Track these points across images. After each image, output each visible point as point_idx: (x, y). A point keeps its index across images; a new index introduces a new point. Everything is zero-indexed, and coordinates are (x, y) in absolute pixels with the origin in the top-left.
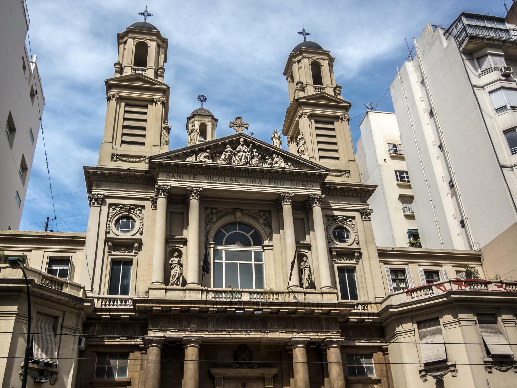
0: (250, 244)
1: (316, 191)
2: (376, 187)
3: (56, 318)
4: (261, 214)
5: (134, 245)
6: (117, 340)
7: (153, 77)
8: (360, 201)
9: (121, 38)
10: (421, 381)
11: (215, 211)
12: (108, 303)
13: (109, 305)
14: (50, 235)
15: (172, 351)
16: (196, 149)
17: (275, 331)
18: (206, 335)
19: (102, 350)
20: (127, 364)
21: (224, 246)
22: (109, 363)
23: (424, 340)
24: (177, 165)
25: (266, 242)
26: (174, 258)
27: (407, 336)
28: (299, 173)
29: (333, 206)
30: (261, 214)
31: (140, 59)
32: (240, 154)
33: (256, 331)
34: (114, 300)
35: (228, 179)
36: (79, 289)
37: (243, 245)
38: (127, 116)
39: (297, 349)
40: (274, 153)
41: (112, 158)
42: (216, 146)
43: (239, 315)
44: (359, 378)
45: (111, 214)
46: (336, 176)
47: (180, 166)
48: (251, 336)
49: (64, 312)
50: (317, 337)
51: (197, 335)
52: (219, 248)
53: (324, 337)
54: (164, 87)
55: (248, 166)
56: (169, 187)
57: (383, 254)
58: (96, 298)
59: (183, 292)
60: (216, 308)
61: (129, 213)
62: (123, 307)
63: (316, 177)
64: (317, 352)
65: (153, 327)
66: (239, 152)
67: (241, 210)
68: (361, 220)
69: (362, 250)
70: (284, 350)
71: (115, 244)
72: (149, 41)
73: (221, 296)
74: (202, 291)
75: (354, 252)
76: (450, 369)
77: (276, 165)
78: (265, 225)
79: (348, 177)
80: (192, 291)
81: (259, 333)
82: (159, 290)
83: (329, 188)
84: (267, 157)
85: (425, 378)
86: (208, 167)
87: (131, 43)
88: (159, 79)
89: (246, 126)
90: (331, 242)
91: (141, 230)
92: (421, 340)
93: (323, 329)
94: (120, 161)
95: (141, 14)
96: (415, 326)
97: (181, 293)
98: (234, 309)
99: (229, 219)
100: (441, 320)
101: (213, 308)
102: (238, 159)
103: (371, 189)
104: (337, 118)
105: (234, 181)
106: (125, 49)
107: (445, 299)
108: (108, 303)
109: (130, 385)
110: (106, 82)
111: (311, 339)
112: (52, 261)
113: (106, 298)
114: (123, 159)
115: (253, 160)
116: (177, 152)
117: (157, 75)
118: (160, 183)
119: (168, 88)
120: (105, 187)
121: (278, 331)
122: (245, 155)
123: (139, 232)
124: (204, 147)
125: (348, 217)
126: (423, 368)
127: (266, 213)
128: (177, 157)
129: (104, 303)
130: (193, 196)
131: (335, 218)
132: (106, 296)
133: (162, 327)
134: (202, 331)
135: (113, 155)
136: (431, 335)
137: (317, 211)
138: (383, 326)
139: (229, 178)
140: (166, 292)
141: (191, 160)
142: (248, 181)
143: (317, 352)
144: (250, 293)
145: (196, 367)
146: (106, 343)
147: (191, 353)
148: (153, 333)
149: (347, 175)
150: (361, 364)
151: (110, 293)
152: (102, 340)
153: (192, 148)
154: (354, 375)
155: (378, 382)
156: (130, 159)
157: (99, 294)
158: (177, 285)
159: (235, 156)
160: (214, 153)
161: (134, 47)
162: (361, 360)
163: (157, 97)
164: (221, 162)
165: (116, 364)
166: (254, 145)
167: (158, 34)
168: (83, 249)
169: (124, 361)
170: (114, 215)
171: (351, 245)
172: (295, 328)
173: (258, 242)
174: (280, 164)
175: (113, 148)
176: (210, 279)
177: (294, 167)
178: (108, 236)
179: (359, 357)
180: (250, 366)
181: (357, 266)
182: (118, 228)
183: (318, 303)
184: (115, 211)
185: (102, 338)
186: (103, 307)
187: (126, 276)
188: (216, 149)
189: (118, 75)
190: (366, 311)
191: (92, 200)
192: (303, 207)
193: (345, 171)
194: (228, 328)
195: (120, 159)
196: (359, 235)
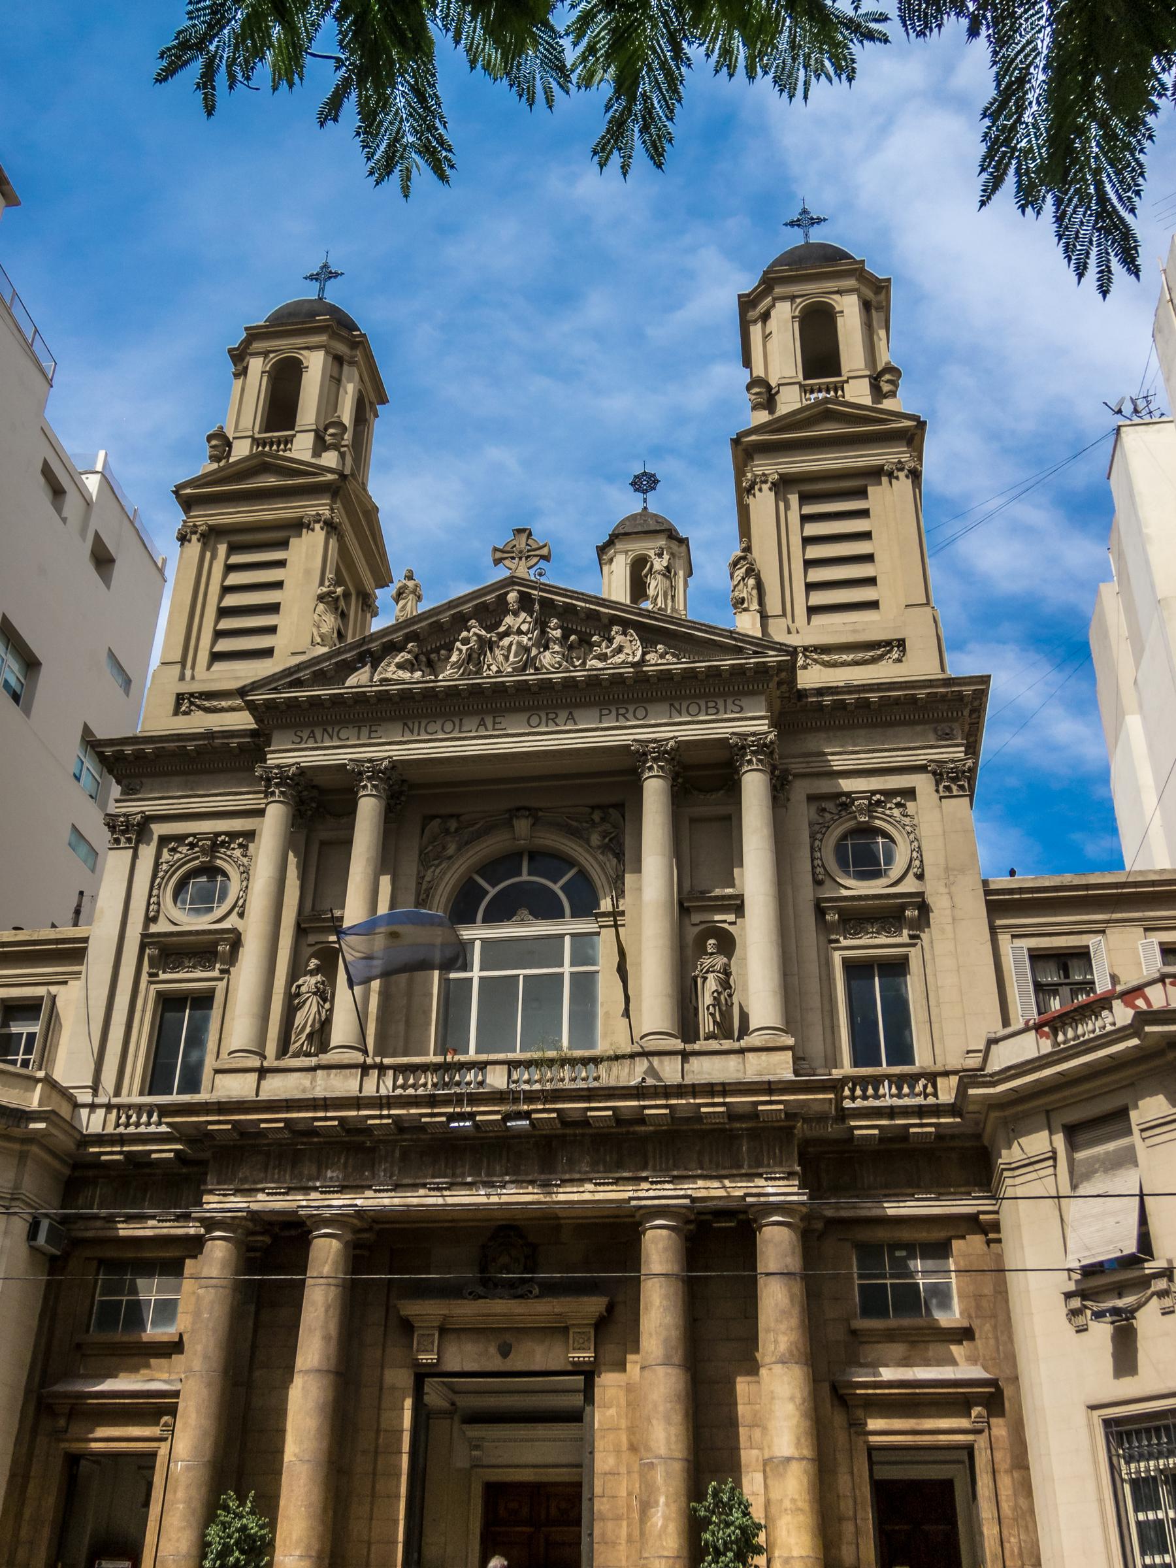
0: (560, 915)
1: (752, 722)
4: (596, 817)
5: (217, 949)
6: (151, 1223)
7: (867, 401)
8: (932, 736)
9: (239, 356)
10: (1069, 1330)
11: (453, 825)
12: (134, 1119)
13: (149, 1124)
14: (1075, 883)
15: (274, 1249)
16: (374, 646)
17: (582, 1181)
18: (368, 1200)
19: (111, 1253)
20: (178, 1290)
21: (479, 928)
22: (134, 1291)
23: (1085, 1189)
24: (315, 702)
25: (606, 905)
26: (308, 978)
27: (1033, 1176)
28: (689, 675)
29: (838, 763)
30: (596, 817)
31: (820, 358)
32: (506, 642)
33: (518, 1182)
34: (877, 1081)
35: (470, 723)
36: (32, 1083)
37: (537, 918)
38: (812, 529)
39: (649, 1234)
40: (615, 620)
41: (178, 704)
42: (437, 627)
43: (458, 1135)
44: (906, 1322)
45: (165, 867)
46: (856, 663)
47: (653, 680)
48: (504, 1199)
50: (722, 1193)
51: (339, 1201)
53: (740, 1193)
54: (330, 477)
55: (530, 676)
56: (671, 743)
57: (1000, 905)
58: (84, 1106)
59: (309, 1075)
60: (389, 1116)
61: (214, 857)
63: (766, 674)
64: (718, 1245)
65: (219, 1183)
66: (507, 634)
67: (533, 813)
68: (936, 796)
69: (930, 900)
70: (618, 1235)
71: (167, 951)
72: (836, 297)
73: (422, 1081)
74: (365, 1069)
75: (903, 908)
76: (1153, 1289)
77: (619, 658)
78: (605, 848)
79: (899, 661)
80: (334, 1071)
81: (530, 1189)
82: (240, 1075)
83: (820, 707)
84: (595, 638)
85: (1080, 1320)
86: (406, 696)
87: (784, 315)
88: (888, 404)
89: (544, 552)
90: (828, 883)
91: (241, 902)
92: (1074, 1187)
93: (740, 1167)
94: (201, 712)
95: (792, 224)
96: (1059, 1140)
97: (304, 1079)
98: (444, 1119)
99: (493, 845)
100: (1134, 1115)
101: (381, 1117)
102: (501, 658)
103: (967, 690)
104: (876, 473)
105: (490, 726)
106: (766, 337)
107: (1135, 1042)
109: (181, 1352)
110: (736, 442)
111: (693, 1200)
113: (130, 1106)
114: (207, 704)
115: (547, 653)
116: (318, 663)
117: (877, 393)
118: (273, 760)
119: (921, 425)
120: (151, 791)
121: (590, 1180)
122: (519, 644)
124: (398, 637)
125: (889, 794)
126: (1072, 1287)
127: (611, 810)
128: (321, 678)
129: (123, 1120)
130: (750, 762)
131: (844, 802)
132: (137, 1099)
133: (244, 1180)
134: (359, 1188)
135: (180, 698)
136: (1106, 1171)
137: (754, 786)
138: (964, 1152)
139: (476, 720)
141: (359, 679)
142: (535, 720)
143: (718, 1245)
144: (512, 1065)
145: (331, 1296)
146: (122, 1233)
147: (326, 1254)
148: (216, 1198)
149: (895, 655)
150: (911, 1274)
152: (111, 1225)
153: (361, 645)
154: (883, 1313)
155: (965, 1334)
156: (223, 704)
158: (308, 1055)
159: (491, 650)
160: (432, 651)
161: (796, 325)
162: (911, 1264)
163: (894, 459)
164: (449, 675)
165: (150, 1291)
166: (546, 607)
167: (859, 272)
168: (80, 973)
169: (171, 1281)
170: (174, 867)
171: (891, 885)
172: (644, 1168)
173: (585, 906)
174: (626, 651)
176: (428, 1029)
177: (674, 655)
178: (154, 929)
179: (904, 1253)
180: (516, 1289)
181: (221, 986)
182: (184, 902)
183: (712, 1085)
184: (177, 856)
185: (110, 1219)
186: (121, 1130)
187: (197, 1040)
188: (430, 637)
189: (763, 417)
190: (931, 1100)
191: (942, 779)
192: (705, 783)
193: (888, 643)
194: (434, 1177)
195: (198, 707)
196: (924, 848)
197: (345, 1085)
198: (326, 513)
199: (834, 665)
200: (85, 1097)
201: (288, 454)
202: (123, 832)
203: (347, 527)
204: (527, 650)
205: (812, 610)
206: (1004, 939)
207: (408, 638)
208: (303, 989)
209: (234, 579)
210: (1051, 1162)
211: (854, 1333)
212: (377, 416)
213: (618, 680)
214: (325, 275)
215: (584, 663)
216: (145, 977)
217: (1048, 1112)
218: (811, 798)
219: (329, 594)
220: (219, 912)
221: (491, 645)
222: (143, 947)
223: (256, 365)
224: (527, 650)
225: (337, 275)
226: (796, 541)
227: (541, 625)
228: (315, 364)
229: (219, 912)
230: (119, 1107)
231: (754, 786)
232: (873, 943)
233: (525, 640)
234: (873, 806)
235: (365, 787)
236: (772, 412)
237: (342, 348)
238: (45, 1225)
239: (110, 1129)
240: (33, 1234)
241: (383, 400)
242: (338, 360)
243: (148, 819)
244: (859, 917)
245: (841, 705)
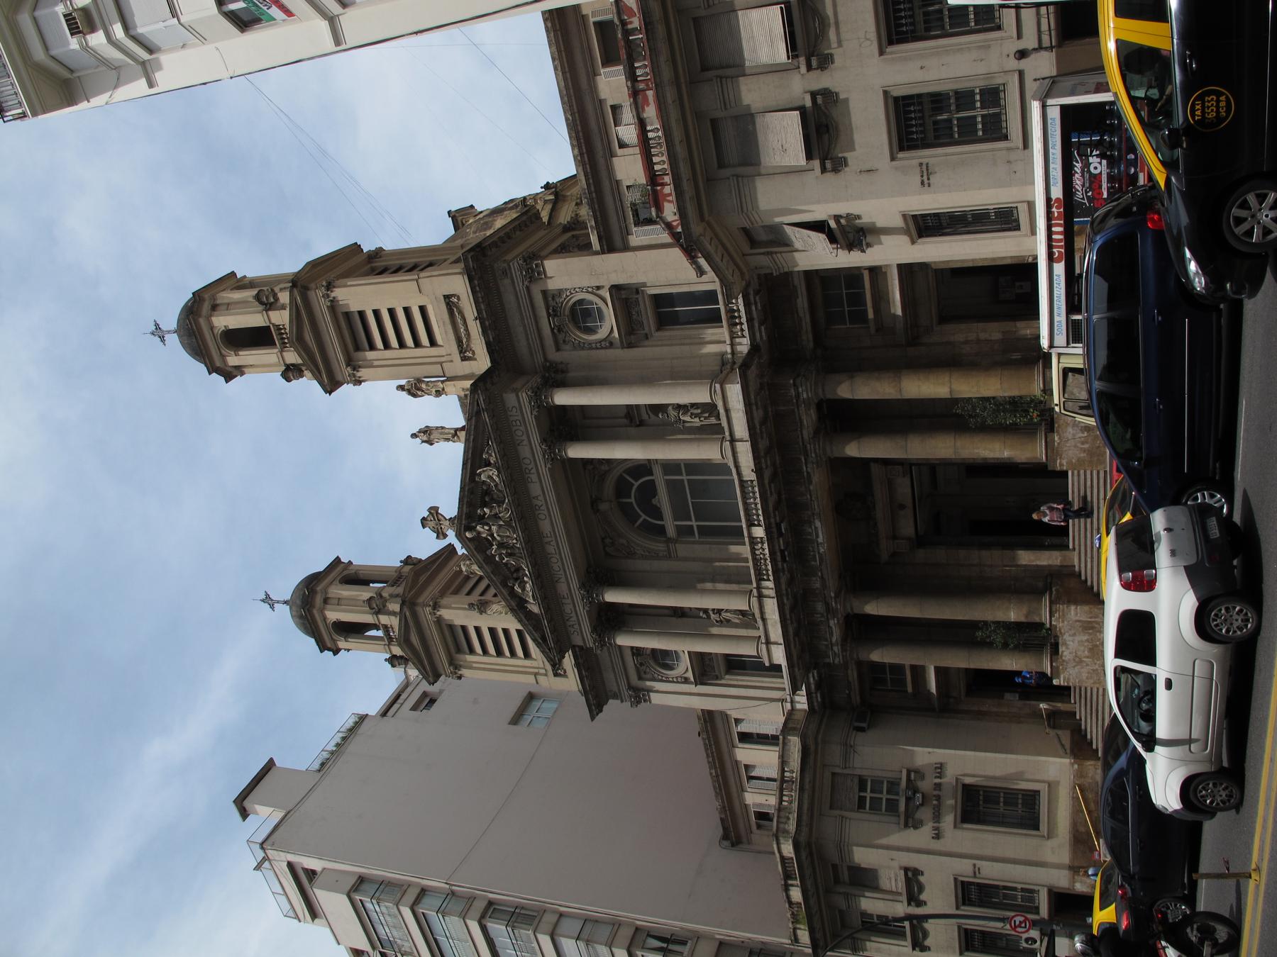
1: (519, 402)
2: (593, 718)
3: (834, 774)
66: (492, 535)
67: (594, 503)
79: (459, 299)
135: (556, 675)
151: (719, 320)
197: (771, 607)
198: (428, 609)
201: (287, 327)
211: (877, 330)
212: (350, 563)
214: (159, 332)
218: (558, 349)
222: (702, 684)
223: (233, 360)
225: (157, 325)
227: (482, 519)
228: (223, 321)
230: (732, 338)
233: (494, 528)
237: (206, 307)
238: (857, 724)
240: (862, 730)
241: (233, 274)
242: (214, 307)
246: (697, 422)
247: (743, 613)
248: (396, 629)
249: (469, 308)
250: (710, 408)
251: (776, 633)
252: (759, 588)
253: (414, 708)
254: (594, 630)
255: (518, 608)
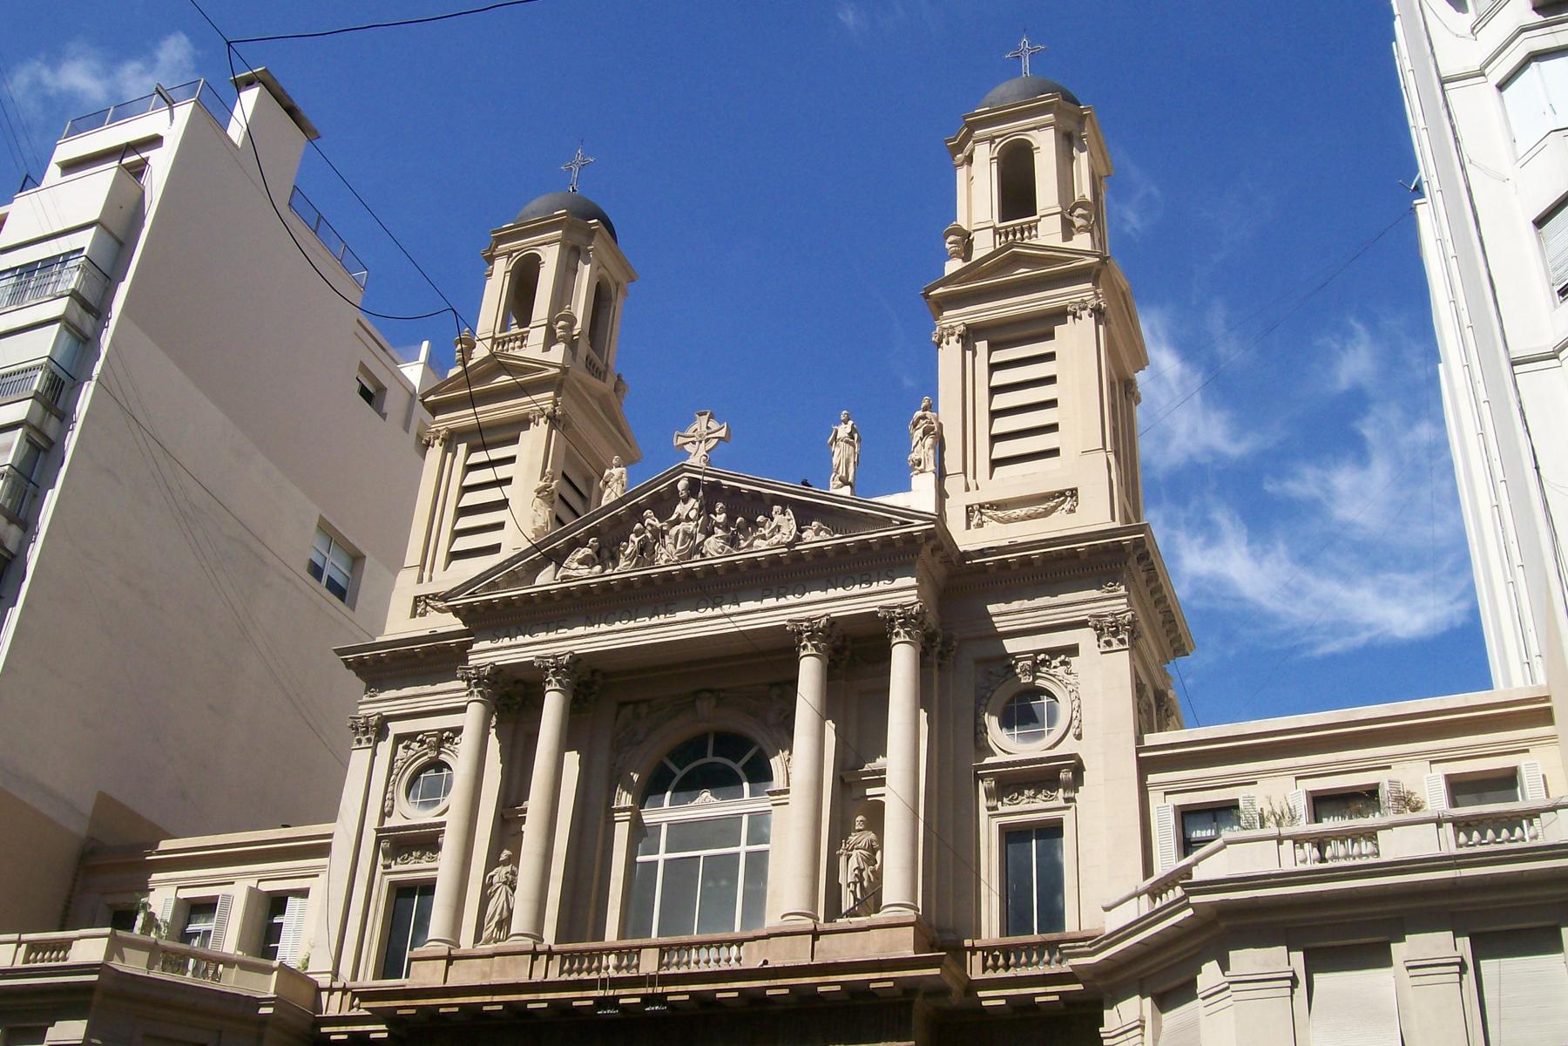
1: (899, 592)
11: (644, 709)
12: (1001, 961)
13: (1007, 967)
32: (673, 531)
34: (1029, 948)
40: (776, 500)
46: (1030, 517)
49: (220, 1032)
52: (649, 816)
55: (696, 563)
61: (440, 753)
62: (1001, 974)
66: (677, 521)
75: (1058, 769)
79: (1072, 511)
86: (586, 590)
99: (679, 730)
107: (1189, 912)
108: (1001, 961)
112: (1322, 803)
113: (994, 948)
115: (712, 539)
118: (473, 660)
122: (685, 533)
123: (1072, 731)
125: (1054, 652)
128: (513, 579)
129: (990, 962)
135: (417, 600)
137: (902, 658)
140: (449, 963)
141: (546, 579)
149: (1067, 506)
157: (355, 977)
161: (995, 167)
164: (624, 568)
175: (967, 489)
178: (389, 823)
182: (415, 797)
192: (856, 654)
193: (1062, 493)
197: (518, 972)
199: (1009, 521)
200: (324, 981)
201: (1034, 241)
202: (365, 733)
203: (1110, 314)
204: (692, 536)
205: (995, 463)
206: (1155, 798)
207: (589, 533)
208: (495, 879)
209: (1001, 378)
210: (1138, 1031)
213: (774, 560)
215: (750, 545)
216: (380, 869)
217: (1141, 980)
218: (978, 662)
219: (544, 489)
220: (1050, 739)
221: (664, 533)
222: (378, 841)
224: (692, 536)
226: (982, 392)
227: (707, 509)
228: (1045, 145)
229: (1050, 739)
231: (902, 658)
232: (1030, 807)
233: (691, 526)
234: (1035, 668)
235: (805, 647)
236: (967, 257)
239: (345, 1012)
243: (384, 721)
244: (1014, 781)
245: (1026, 562)
246: (846, 876)
247: (504, 923)
248: (517, 353)
249: (1058, 525)
250: (871, 898)
251: (462, 975)
252: (550, 954)
253: (363, 368)
254: (498, 670)
255: (548, 553)
